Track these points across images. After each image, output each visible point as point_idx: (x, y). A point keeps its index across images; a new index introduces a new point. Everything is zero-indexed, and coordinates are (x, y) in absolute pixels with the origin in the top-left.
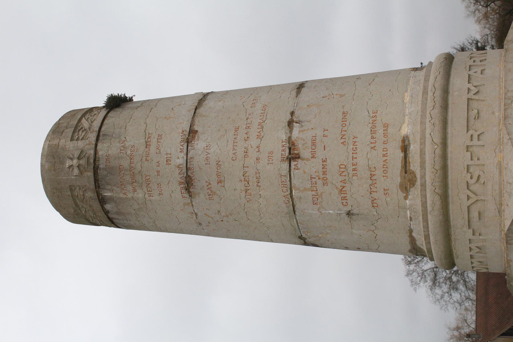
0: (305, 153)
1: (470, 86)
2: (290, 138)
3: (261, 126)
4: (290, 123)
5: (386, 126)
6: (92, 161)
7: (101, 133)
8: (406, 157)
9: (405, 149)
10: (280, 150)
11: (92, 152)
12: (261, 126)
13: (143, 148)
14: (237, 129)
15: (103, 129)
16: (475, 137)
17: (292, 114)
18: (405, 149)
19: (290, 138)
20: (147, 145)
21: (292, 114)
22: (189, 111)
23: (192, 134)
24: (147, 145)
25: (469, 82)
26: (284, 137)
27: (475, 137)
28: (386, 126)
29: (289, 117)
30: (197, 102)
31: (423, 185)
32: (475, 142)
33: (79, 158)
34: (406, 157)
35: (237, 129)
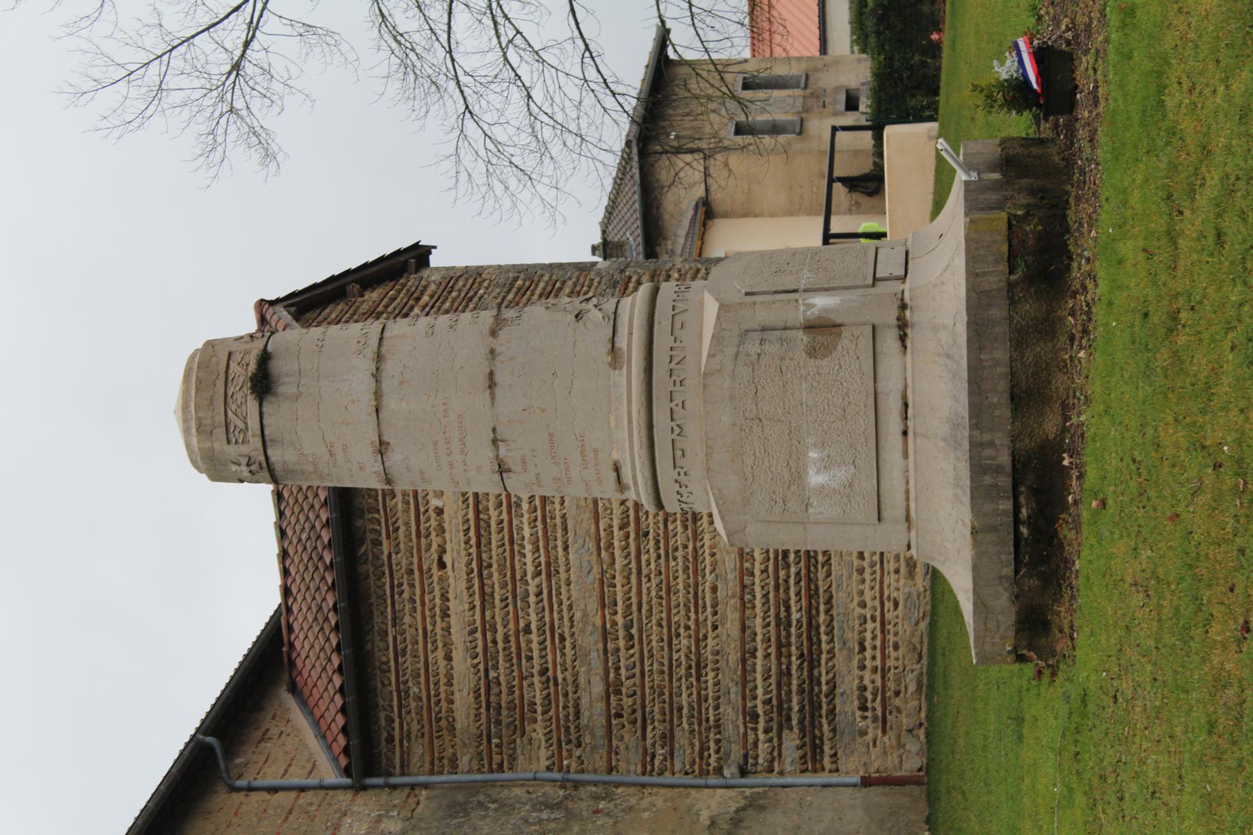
0: (517, 468)
1: (673, 424)
2: (497, 456)
3: (462, 441)
4: (495, 441)
5: (596, 451)
6: (265, 465)
7: (267, 439)
8: (618, 476)
9: (617, 469)
10: (489, 466)
11: (263, 458)
12: (462, 441)
13: (326, 457)
14: (436, 443)
15: (267, 432)
16: (678, 383)
17: (494, 430)
18: (617, 469)
19: (497, 456)
20: (331, 454)
21: (494, 430)
22: (370, 414)
23: (382, 447)
24: (331, 454)
25: (672, 420)
26: (491, 455)
27: (678, 383)
28: (596, 451)
29: (491, 435)
30: (373, 397)
31: (629, 368)
32: (678, 344)
33: (248, 465)
34: (618, 476)
35: (436, 443)
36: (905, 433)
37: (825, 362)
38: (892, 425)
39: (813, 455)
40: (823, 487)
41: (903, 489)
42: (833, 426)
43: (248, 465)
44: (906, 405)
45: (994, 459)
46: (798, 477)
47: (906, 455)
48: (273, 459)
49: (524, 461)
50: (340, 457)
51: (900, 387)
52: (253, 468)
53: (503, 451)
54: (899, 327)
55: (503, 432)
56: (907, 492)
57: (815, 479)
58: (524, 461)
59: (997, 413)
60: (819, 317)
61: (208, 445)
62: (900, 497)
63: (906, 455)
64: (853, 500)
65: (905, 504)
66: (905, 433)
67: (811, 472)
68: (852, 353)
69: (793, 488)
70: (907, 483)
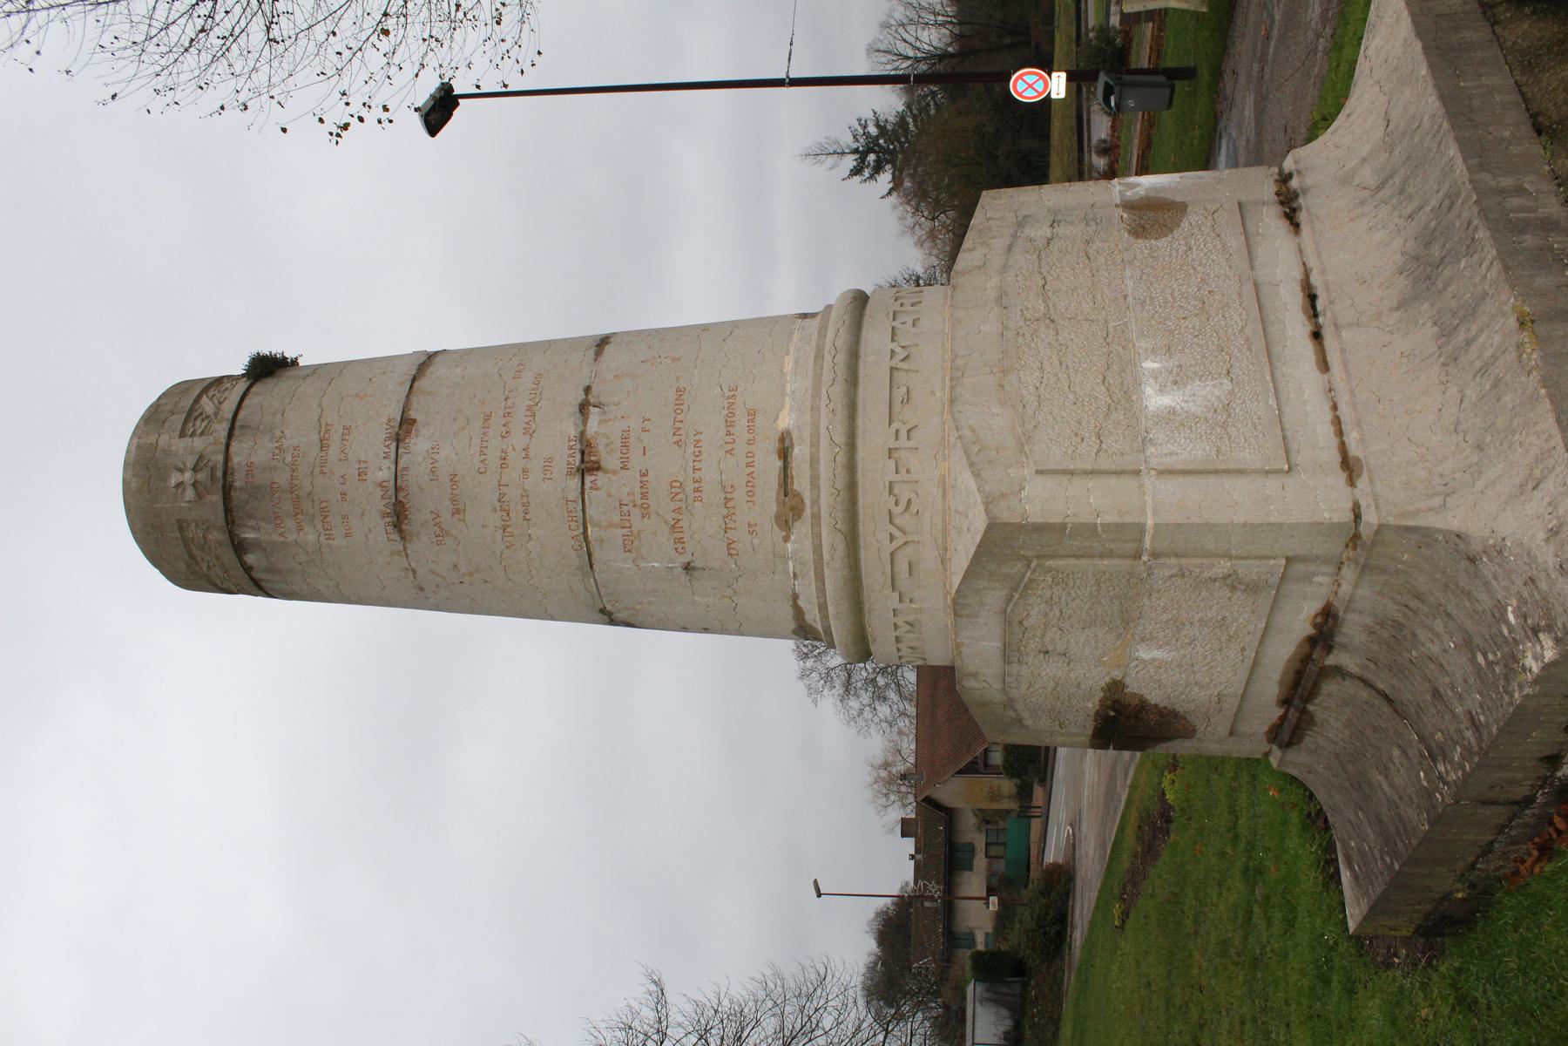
1: (894, 346)
2: (582, 433)
4: (583, 408)
5: (752, 414)
7: (237, 424)
8: (785, 468)
9: (784, 454)
10: (564, 456)
11: (220, 458)
14: (487, 417)
16: (903, 433)
17: (588, 390)
18: (784, 454)
19: (582, 433)
20: (323, 445)
21: (588, 390)
26: (572, 432)
27: (903, 433)
28: (752, 414)
29: (581, 396)
31: (816, 517)
32: (903, 475)
36: (1317, 335)
37: (1163, 242)
38: (1296, 327)
39: (1149, 365)
40: (1172, 411)
41: (1329, 416)
42: (1184, 323)
43: (195, 469)
44: (1312, 298)
45: (1530, 210)
46: (1125, 396)
47: (1324, 366)
48: (236, 460)
49: (625, 444)
50: (333, 452)
51: (1298, 274)
52: (202, 476)
53: (593, 425)
54: (1282, 203)
55: (600, 392)
56: (1337, 422)
57: (1156, 400)
58: (625, 444)
59: (1515, 150)
60: (1147, 197)
61: (152, 439)
62: (1325, 431)
63: (1324, 366)
64: (1231, 430)
65: (1335, 442)
66: (1317, 335)
67: (1149, 391)
68: (1206, 229)
69: (1114, 415)
70: (1335, 407)
